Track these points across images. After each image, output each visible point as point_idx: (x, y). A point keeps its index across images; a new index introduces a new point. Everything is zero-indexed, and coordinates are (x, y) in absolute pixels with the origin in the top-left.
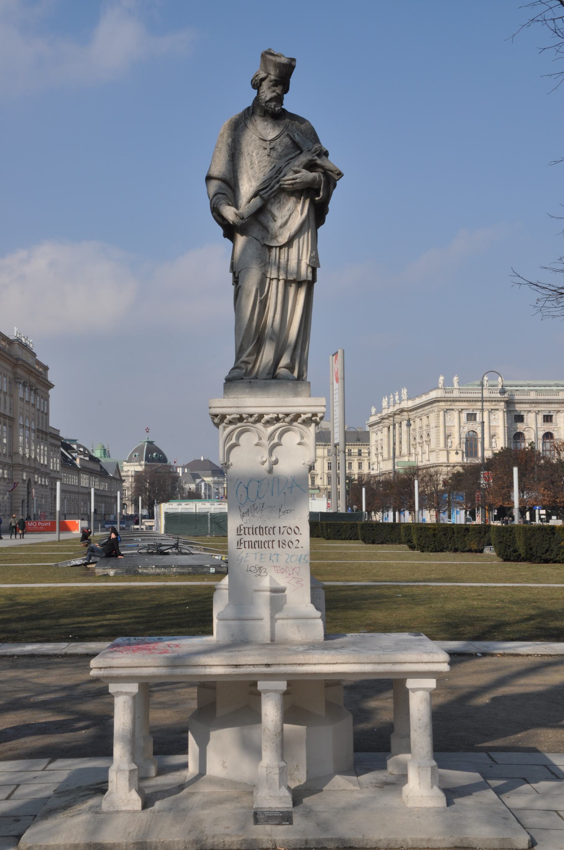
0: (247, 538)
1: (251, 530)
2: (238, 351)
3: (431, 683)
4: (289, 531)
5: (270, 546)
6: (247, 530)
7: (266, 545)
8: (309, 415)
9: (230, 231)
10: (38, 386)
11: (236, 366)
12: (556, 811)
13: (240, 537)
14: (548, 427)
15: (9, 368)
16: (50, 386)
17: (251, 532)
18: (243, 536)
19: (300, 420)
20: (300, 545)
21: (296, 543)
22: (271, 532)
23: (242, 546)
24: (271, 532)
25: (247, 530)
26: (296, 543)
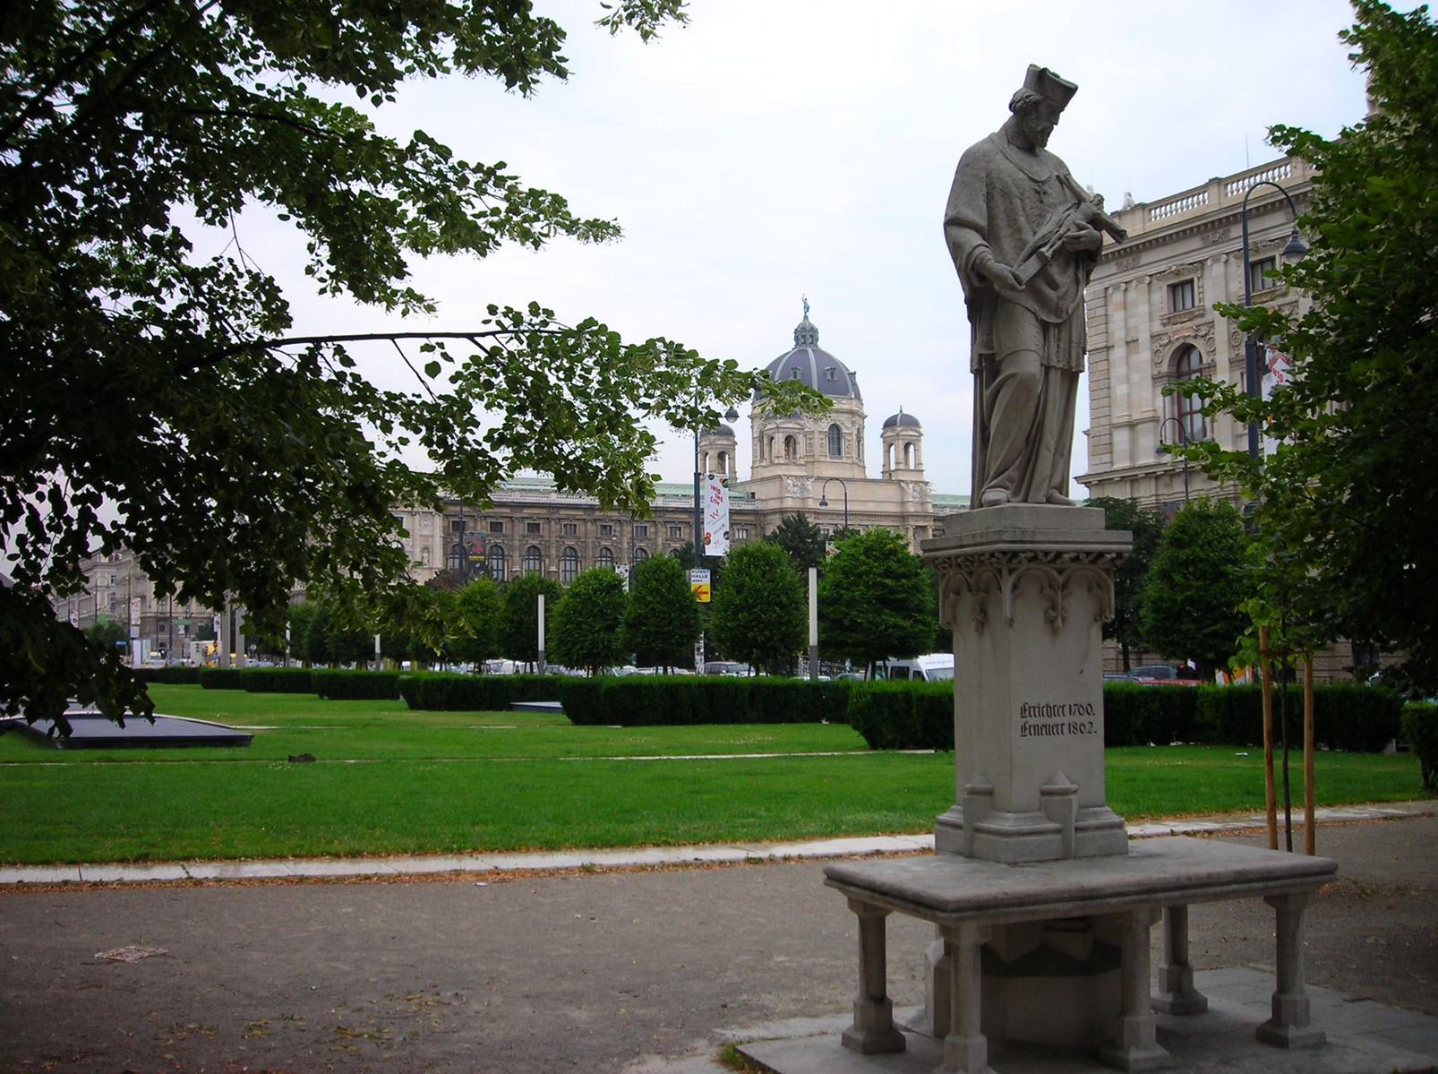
0: (1032, 721)
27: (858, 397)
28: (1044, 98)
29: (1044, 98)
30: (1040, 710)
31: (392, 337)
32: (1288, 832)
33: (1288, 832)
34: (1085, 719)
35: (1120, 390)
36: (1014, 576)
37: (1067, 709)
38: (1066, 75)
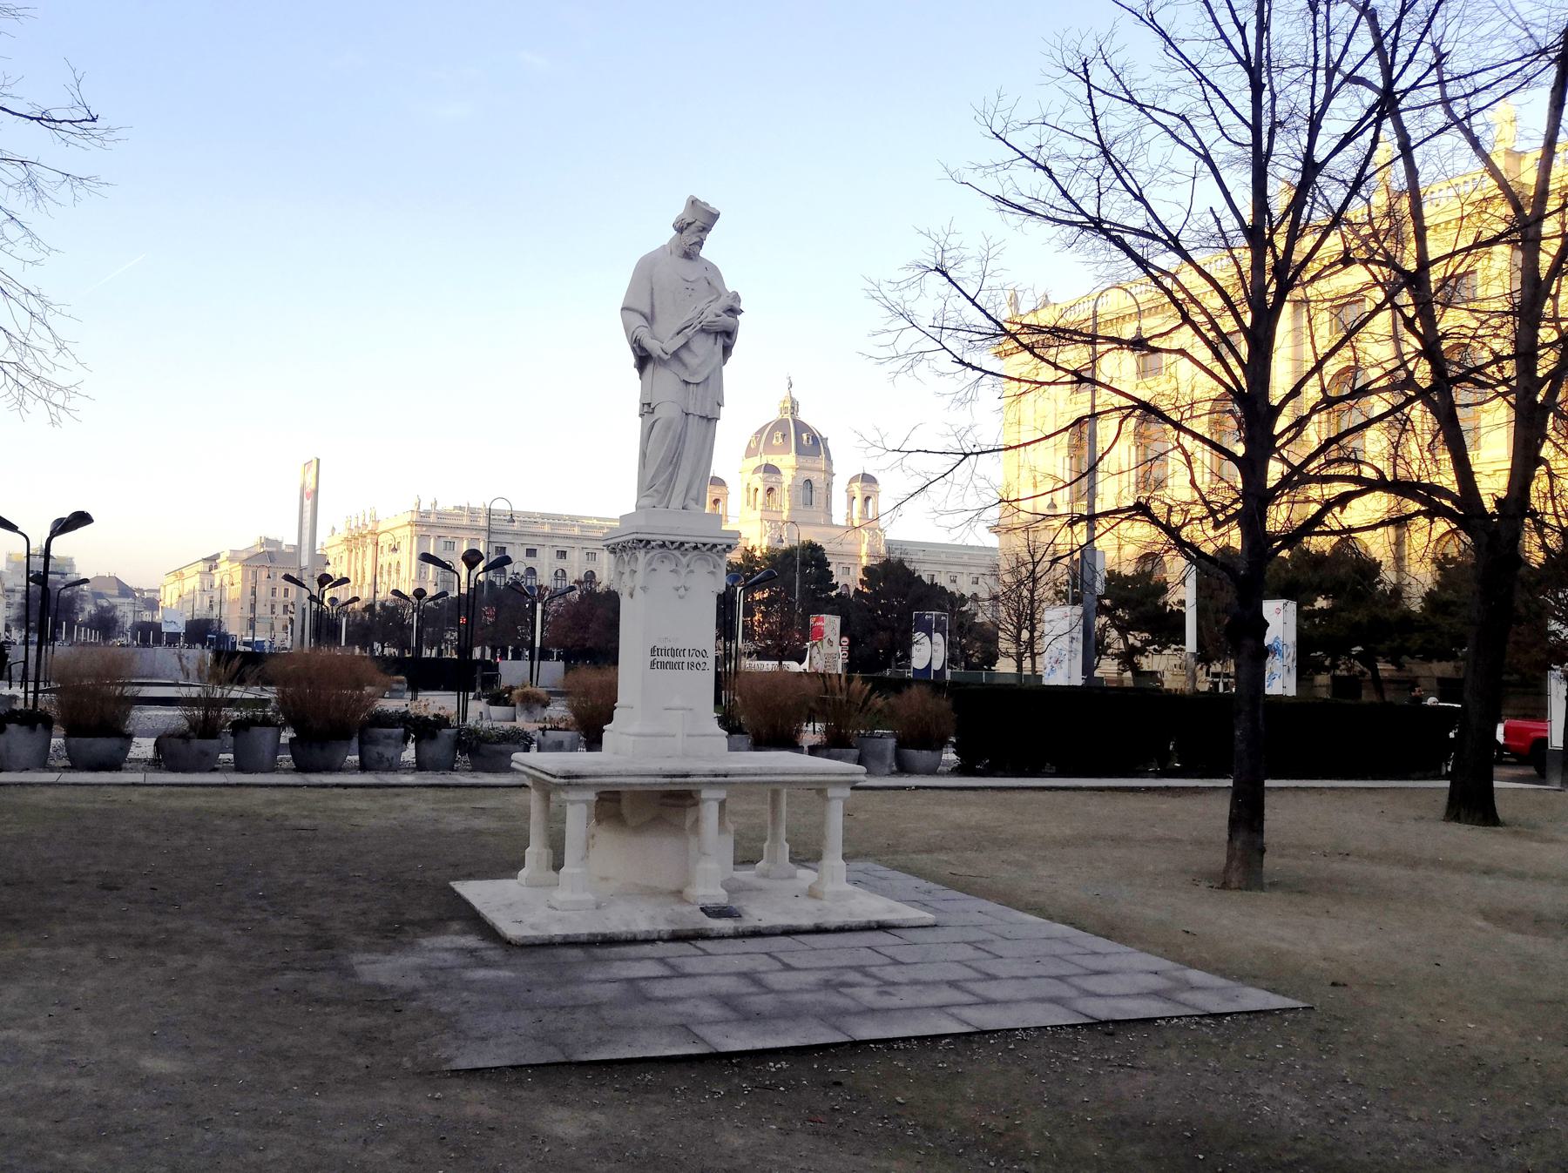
0: (660, 659)
9: (643, 360)
14: (531, 562)
28: (697, 223)
29: (697, 223)
30: (666, 652)
34: (701, 659)
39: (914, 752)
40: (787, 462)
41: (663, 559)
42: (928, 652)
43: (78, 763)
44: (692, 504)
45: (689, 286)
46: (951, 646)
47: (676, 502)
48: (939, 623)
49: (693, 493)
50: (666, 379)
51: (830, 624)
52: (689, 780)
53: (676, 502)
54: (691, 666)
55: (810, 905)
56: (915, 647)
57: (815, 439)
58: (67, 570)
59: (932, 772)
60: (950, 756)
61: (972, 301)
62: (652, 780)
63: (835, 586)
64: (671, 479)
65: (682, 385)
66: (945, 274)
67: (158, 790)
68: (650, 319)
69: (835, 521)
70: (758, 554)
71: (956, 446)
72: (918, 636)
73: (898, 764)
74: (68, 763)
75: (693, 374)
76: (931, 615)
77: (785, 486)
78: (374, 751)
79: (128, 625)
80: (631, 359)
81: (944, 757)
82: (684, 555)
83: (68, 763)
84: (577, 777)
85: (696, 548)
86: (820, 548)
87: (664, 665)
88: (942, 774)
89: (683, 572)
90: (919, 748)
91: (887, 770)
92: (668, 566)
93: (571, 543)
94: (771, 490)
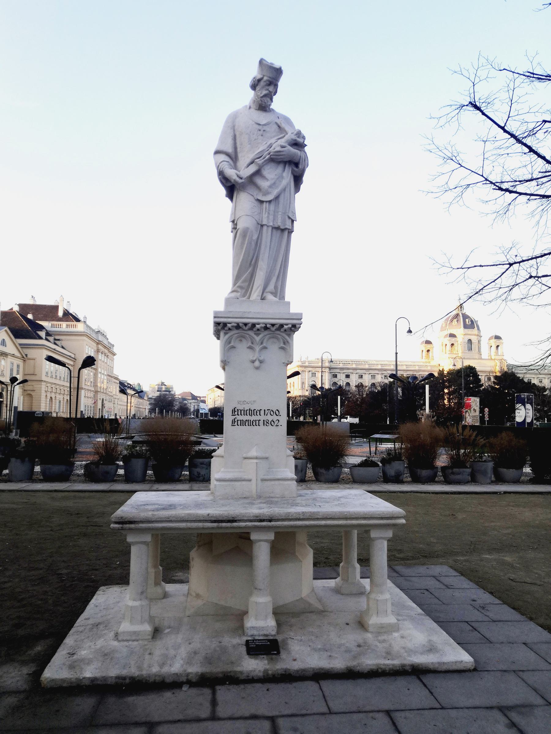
0: (240, 418)
1: (243, 412)
2: (236, 273)
3: (389, 534)
4: (272, 412)
5: (257, 424)
6: (239, 411)
7: (254, 424)
8: (290, 326)
9: (231, 189)
10: (109, 354)
11: (233, 289)
12: (467, 622)
13: (234, 417)
14: (348, 380)
15: (95, 345)
16: (114, 354)
17: (242, 413)
18: (237, 416)
19: (282, 330)
20: (279, 424)
21: (276, 423)
22: (258, 414)
23: (236, 423)
24: (258, 414)
25: (239, 411)
26: (276, 423)
27: (478, 329)
28: (268, 81)
29: (268, 81)
30: (245, 412)
31: (509, 117)
32: (218, 317)
33: (218, 317)
34: (275, 418)
35: (88, 450)
36: (227, 336)
37: (262, 412)
38: (277, 64)
39: (505, 470)
40: (460, 331)
41: (241, 338)
42: (523, 413)
43: (47, 478)
44: (270, 297)
45: (262, 128)
46: (535, 410)
47: (255, 294)
48: (529, 399)
49: (271, 287)
50: (245, 199)
51: (475, 402)
52: (235, 524)
53: (255, 294)
54: (266, 423)
55: (351, 638)
56: (517, 411)
57: (472, 321)
58: (171, 390)
59: (517, 481)
60: (527, 470)
61: (503, 128)
62: (200, 525)
63: (482, 385)
64: (252, 276)
65: (256, 203)
66: (478, 108)
67: (60, 495)
68: (234, 157)
69: (483, 357)
70: (445, 372)
71: (502, 259)
72: (518, 406)
73: (495, 476)
74: (42, 478)
75: (266, 193)
76: (524, 395)
77: (459, 342)
78: (196, 470)
79: (192, 410)
80: (223, 191)
81: (524, 470)
82: (258, 335)
83: (42, 478)
84: (131, 522)
85: (266, 328)
86: (474, 368)
87: (243, 423)
88: (523, 483)
89: (257, 348)
90: (508, 468)
91: (489, 481)
92: (245, 344)
93: (377, 372)
94: (452, 345)
